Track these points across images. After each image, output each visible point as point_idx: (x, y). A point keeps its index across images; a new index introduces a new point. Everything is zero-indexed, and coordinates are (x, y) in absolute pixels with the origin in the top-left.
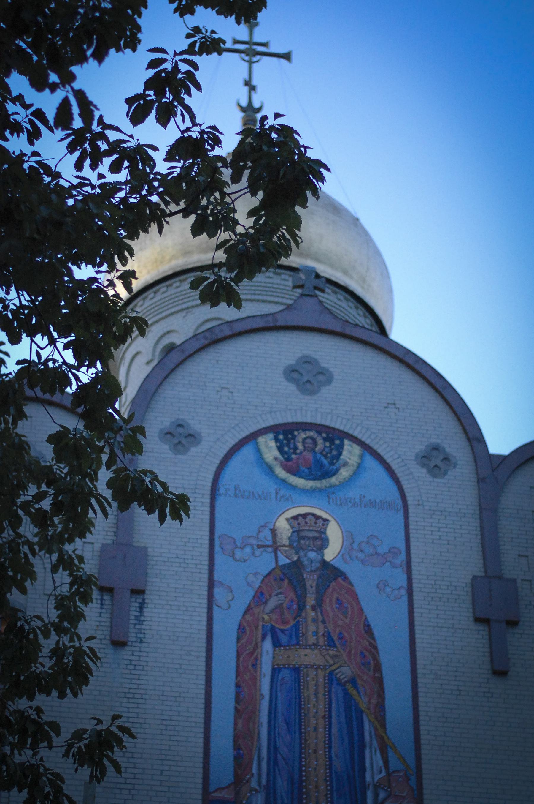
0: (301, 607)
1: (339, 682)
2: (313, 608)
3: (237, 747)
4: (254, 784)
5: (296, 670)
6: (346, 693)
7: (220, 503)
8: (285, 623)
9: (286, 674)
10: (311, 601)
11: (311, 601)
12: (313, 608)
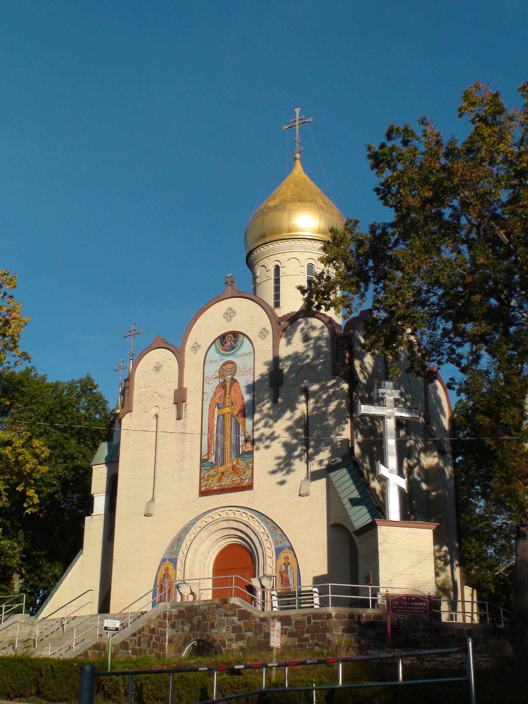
0: (225, 395)
1: (234, 416)
2: (228, 394)
3: (208, 443)
4: (212, 452)
5: (223, 415)
6: (236, 419)
7: (206, 366)
8: (221, 401)
9: (221, 417)
10: (228, 392)
11: (228, 392)
12: (228, 394)
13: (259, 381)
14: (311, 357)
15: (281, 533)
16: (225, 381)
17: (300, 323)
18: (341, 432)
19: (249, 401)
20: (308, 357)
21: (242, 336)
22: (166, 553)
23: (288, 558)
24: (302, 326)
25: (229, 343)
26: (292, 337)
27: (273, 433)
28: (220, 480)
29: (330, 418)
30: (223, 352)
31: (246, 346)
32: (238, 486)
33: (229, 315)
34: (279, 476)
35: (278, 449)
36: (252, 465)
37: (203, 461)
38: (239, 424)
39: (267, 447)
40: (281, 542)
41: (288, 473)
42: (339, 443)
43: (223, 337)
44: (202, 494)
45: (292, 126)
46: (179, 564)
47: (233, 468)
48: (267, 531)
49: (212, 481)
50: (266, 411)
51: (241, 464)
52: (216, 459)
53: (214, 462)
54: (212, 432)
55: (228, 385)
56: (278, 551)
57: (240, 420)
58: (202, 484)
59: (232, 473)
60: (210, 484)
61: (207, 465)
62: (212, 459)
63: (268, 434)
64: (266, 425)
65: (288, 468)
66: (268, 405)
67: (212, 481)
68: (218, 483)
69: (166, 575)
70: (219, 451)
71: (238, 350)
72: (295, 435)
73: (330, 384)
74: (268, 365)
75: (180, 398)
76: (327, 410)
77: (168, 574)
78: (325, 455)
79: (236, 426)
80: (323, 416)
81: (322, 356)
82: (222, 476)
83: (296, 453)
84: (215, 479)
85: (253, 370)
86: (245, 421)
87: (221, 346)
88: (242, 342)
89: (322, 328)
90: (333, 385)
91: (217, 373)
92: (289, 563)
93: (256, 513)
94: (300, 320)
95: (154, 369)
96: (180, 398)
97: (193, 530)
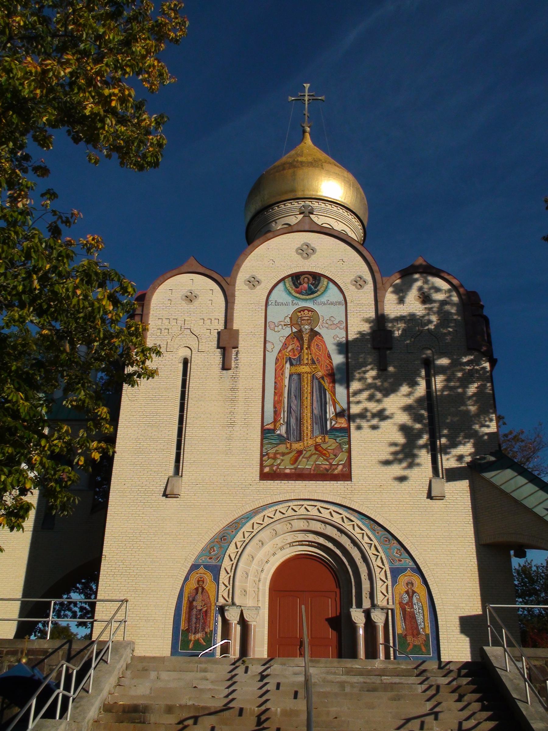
0: (302, 349)
1: (317, 378)
2: (307, 349)
3: (275, 407)
4: (282, 422)
7: (269, 308)
8: (295, 356)
9: (295, 377)
10: (306, 346)
11: (306, 346)
12: (307, 349)
13: (355, 340)
14: (435, 323)
15: (399, 547)
16: (300, 331)
17: (416, 280)
18: (487, 423)
19: (342, 364)
20: (430, 322)
21: (326, 280)
22: (198, 557)
23: (412, 584)
24: (419, 284)
25: (305, 285)
26: (406, 294)
27: (383, 411)
28: (295, 461)
29: (469, 402)
30: (298, 295)
31: (333, 293)
32: (326, 472)
33: (306, 251)
34: (397, 470)
35: (390, 433)
36: (347, 446)
37: (266, 433)
38: (325, 390)
39: (374, 427)
40: (400, 561)
41: (411, 466)
42: (486, 437)
43: (296, 278)
44: (264, 476)
45: (300, 100)
46: (223, 577)
47: (317, 447)
48: (375, 542)
49: (282, 460)
50: (370, 381)
51: (329, 444)
52: (287, 432)
53: (285, 436)
54: (281, 395)
55: (306, 337)
56: (396, 573)
57: (327, 384)
58: (265, 464)
59: (315, 454)
60: (279, 464)
61: (272, 438)
62: (282, 430)
63: (374, 411)
64: (371, 398)
65: (409, 460)
66: (373, 373)
67: (282, 460)
68: (292, 464)
69: (200, 590)
70: (293, 421)
71: (319, 295)
72: (417, 418)
73: (465, 360)
74: (370, 323)
75: (227, 343)
76: (465, 393)
77: (203, 589)
78: (466, 449)
79: (320, 392)
80: (462, 399)
81: (452, 325)
82: (299, 456)
83: (422, 442)
84: (287, 458)
85: (344, 324)
86: (334, 387)
87: (294, 287)
88: (327, 287)
89: (449, 291)
90: (469, 363)
91: (288, 320)
92: (414, 592)
93: (356, 514)
94: (417, 276)
95: (184, 298)
96: (227, 343)
97: (247, 527)
